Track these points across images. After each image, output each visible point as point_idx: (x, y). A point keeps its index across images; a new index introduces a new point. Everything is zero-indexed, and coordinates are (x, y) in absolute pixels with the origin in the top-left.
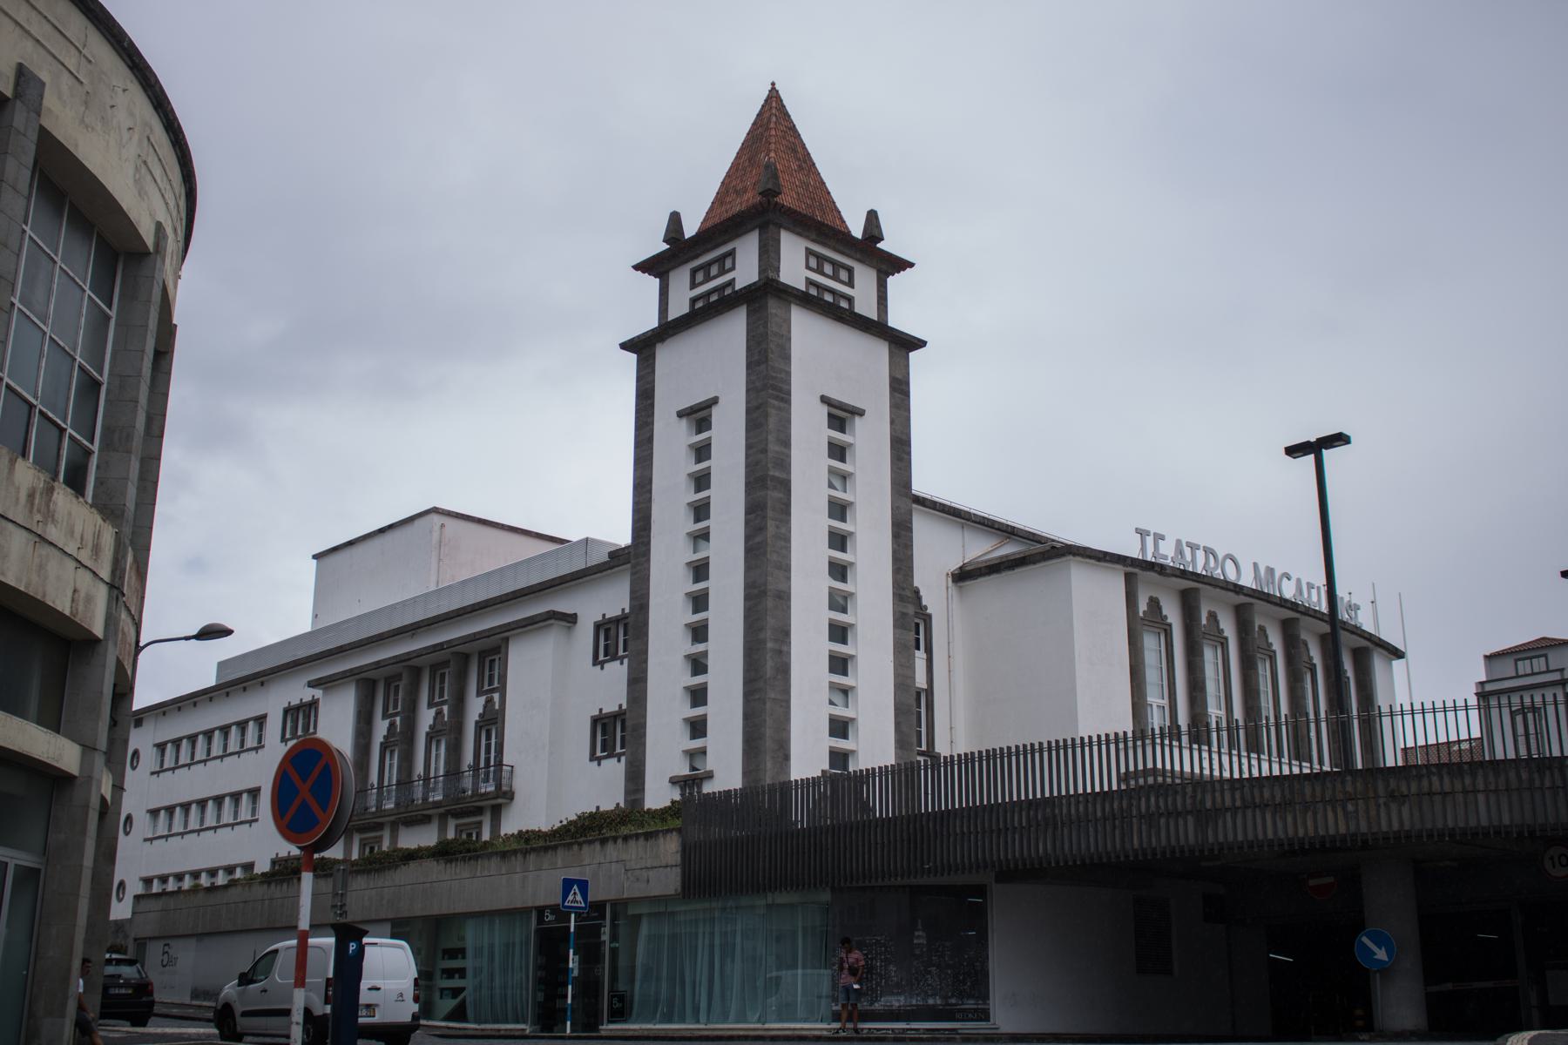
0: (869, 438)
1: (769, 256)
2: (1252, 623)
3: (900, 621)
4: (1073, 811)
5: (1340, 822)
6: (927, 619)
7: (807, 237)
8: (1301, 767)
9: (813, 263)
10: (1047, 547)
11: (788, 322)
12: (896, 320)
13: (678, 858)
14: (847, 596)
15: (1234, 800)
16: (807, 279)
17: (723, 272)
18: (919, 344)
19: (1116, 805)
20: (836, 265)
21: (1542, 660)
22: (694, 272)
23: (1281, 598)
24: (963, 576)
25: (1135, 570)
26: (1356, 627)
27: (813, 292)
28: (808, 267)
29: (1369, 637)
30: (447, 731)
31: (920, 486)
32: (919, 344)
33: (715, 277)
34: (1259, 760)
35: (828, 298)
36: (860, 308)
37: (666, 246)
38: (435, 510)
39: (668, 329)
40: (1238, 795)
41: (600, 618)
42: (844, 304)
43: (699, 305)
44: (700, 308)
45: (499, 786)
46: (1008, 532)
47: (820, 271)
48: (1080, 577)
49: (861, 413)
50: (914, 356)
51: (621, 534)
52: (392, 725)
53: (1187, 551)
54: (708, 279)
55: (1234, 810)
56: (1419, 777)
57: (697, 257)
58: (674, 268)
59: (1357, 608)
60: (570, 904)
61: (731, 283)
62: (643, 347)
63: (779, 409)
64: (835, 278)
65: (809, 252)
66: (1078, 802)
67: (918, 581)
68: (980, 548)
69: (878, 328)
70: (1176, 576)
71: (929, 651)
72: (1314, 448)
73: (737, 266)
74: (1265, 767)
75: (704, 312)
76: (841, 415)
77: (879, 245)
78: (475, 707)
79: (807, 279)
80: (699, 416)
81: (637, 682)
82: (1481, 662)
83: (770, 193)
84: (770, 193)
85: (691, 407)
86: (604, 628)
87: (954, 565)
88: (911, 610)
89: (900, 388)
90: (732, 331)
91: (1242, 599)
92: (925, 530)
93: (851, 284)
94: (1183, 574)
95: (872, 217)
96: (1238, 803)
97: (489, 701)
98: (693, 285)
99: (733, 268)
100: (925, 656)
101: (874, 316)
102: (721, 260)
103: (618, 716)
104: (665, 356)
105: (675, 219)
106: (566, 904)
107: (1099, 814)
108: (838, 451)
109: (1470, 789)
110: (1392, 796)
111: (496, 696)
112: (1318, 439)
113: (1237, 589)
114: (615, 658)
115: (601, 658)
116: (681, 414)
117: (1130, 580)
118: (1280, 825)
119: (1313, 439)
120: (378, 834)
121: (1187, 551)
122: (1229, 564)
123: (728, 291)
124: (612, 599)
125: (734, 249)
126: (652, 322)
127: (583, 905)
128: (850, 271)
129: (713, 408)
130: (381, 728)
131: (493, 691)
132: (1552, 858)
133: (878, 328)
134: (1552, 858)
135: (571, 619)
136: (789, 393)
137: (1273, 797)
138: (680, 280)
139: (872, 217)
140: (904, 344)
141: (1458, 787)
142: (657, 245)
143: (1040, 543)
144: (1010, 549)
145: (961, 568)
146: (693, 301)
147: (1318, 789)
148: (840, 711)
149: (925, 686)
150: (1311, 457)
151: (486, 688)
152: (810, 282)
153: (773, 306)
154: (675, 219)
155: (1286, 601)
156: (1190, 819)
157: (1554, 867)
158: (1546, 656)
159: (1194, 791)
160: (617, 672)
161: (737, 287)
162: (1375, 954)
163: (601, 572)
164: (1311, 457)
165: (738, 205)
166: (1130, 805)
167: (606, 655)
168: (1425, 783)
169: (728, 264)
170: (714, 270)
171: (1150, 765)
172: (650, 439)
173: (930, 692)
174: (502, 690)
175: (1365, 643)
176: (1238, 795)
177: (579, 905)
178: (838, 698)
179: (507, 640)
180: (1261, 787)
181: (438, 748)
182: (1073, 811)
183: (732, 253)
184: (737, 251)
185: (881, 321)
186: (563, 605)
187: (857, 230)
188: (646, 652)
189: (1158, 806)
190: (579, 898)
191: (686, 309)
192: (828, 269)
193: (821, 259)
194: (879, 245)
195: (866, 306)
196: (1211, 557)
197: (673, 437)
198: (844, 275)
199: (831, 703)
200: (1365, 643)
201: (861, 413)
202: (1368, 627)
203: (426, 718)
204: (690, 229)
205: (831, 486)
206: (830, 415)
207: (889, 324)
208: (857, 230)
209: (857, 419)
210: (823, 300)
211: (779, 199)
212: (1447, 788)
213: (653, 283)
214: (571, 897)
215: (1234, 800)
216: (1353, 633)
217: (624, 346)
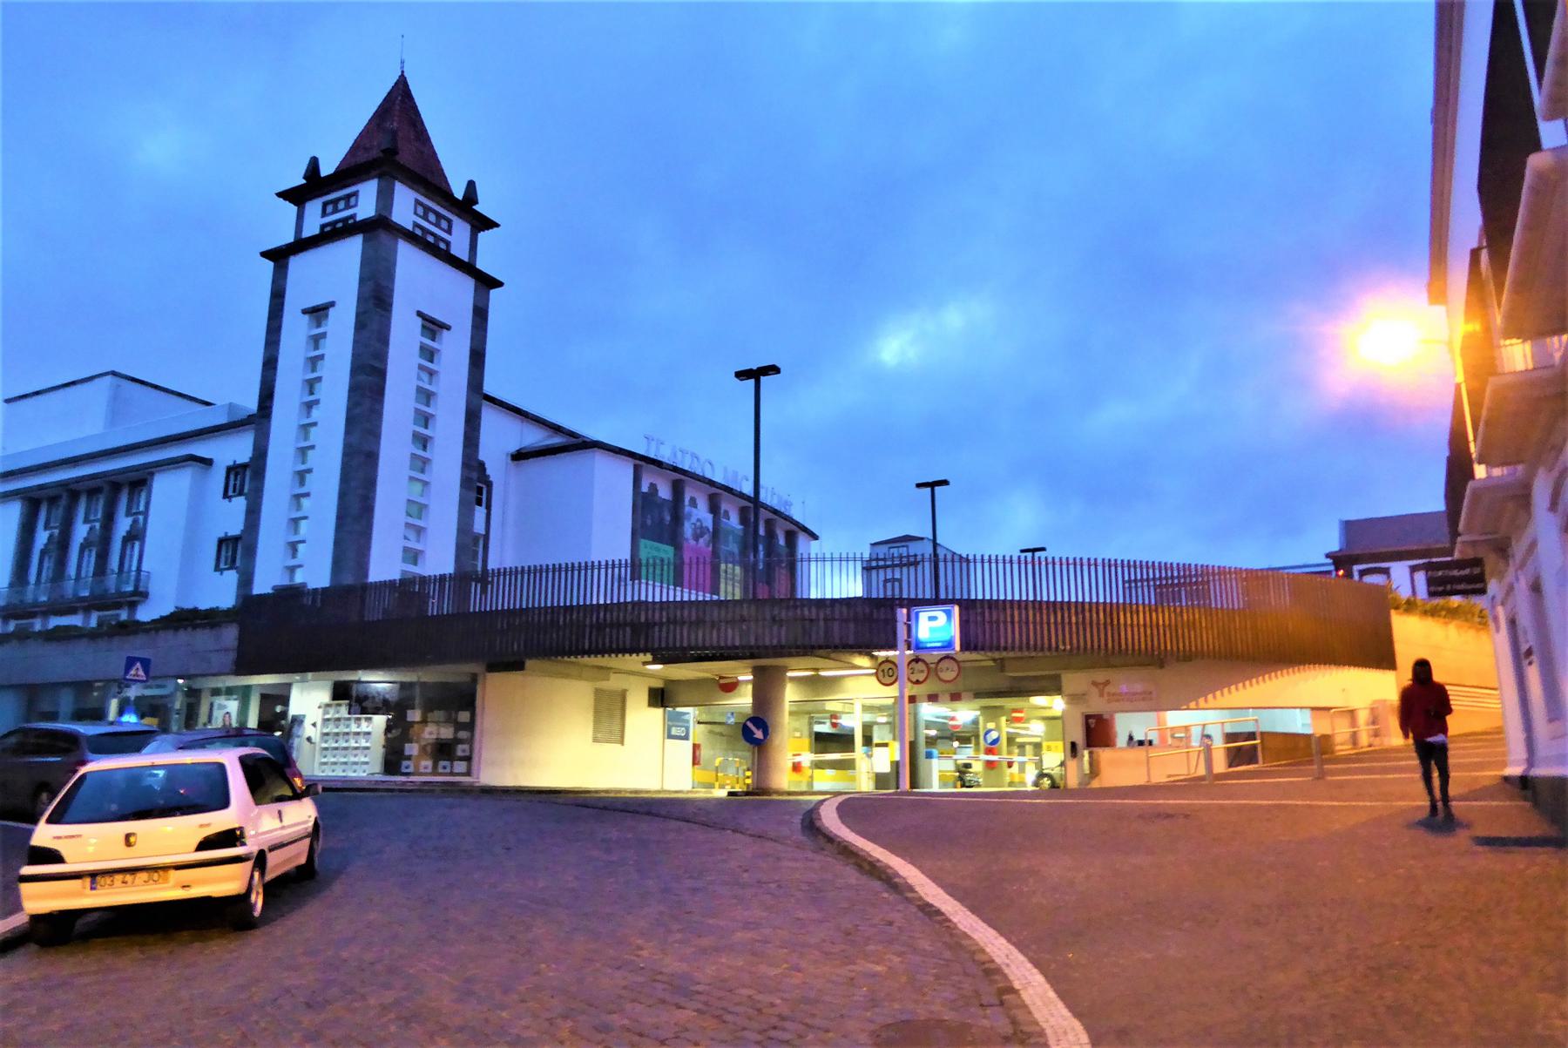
0: (454, 349)
1: (385, 198)
2: (719, 508)
3: (466, 483)
4: (542, 619)
5: (1195, 764)
6: (489, 485)
7: (417, 191)
8: (704, 596)
9: (420, 210)
10: (580, 440)
11: (395, 251)
12: (481, 265)
13: (236, 643)
14: (426, 461)
15: (661, 617)
16: (414, 222)
17: (348, 207)
18: (500, 284)
19: (574, 617)
20: (439, 216)
21: (905, 549)
22: (325, 205)
23: (741, 492)
24: (519, 456)
25: (642, 462)
26: (788, 516)
27: (419, 232)
28: (415, 213)
29: (796, 524)
30: (101, 543)
31: (489, 388)
32: (500, 284)
33: (341, 210)
34: (682, 591)
35: (431, 239)
36: (454, 251)
37: (304, 181)
38: (114, 373)
39: (301, 245)
40: (664, 614)
41: (231, 463)
42: (443, 246)
43: (328, 229)
44: (328, 232)
45: (136, 586)
46: (557, 429)
47: (425, 218)
48: (600, 460)
49: (448, 328)
50: (494, 293)
51: (251, 404)
52: (51, 536)
53: (679, 454)
54: (336, 211)
55: (661, 624)
56: (795, 607)
57: (328, 193)
58: (310, 199)
59: (791, 505)
60: (131, 677)
61: (353, 216)
62: (279, 257)
63: (382, 316)
64: (437, 225)
65: (417, 202)
66: (540, 613)
67: (483, 455)
68: (534, 437)
69: (468, 268)
70: (670, 470)
71: (489, 507)
72: (753, 374)
73: (359, 203)
74: (686, 595)
75: (330, 235)
76: (433, 326)
77: (474, 207)
78: (123, 525)
79: (414, 222)
80: (318, 312)
81: (253, 515)
82: (869, 546)
83: (391, 152)
84: (391, 152)
85: (314, 307)
86: (235, 470)
87: (513, 448)
88: (475, 475)
89: (480, 315)
90: (352, 249)
91: (714, 490)
92: (489, 416)
93: (449, 231)
94: (675, 469)
95: (471, 185)
96: (664, 620)
97: (135, 522)
98: (324, 214)
99: (356, 205)
100: (485, 511)
101: (465, 258)
102: (348, 197)
103: (236, 539)
104: (296, 263)
105: (314, 164)
106: (128, 677)
107: (561, 623)
108: (429, 354)
109: (830, 617)
110: (774, 619)
111: (141, 518)
112: (758, 368)
113: (712, 483)
114: (241, 493)
115: (230, 493)
116: (305, 312)
117: (637, 470)
118: (693, 637)
119: (755, 368)
120: (31, 621)
121: (679, 454)
122: (708, 467)
123: (351, 221)
124: (238, 449)
125: (358, 191)
126: (288, 237)
127: (145, 679)
128: (450, 222)
129: (331, 309)
130: (42, 537)
131: (139, 513)
132: (883, 671)
133: (468, 268)
134: (883, 671)
135: (208, 462)
136: (391, 305)
137: (690, 617)
138: (314, 208)
139: (471, 185)
140: (486, 283)
141: (822, 616)
142: (298, 180)
143: (574, 437)
144: (557, 440)
145: (518, 451)
146: (323, 226)
147: (723, 612)
148: (412, 545)
149: (484, 533)
150: (752, 382)
151: (134, 511)
152: (416, 225)
153: (383, 236)
154: (314, 164)
155: (744, 494)
156: (628, 630)
157: (884, 676)
158: (907, 547)
159: (633, 608)
160: (240, 503)
161: (358, 219)
162: (754, 734)
163: (242, 426)
164: (752, 382)
165: (362, 158)
166: (585, 617)
167: (234, 491)
168: (799, 611)
169: (353, 200)
170: (341, 205)
171: (643, 598)
172: (279, 328)
173: (486, 537)
174: (146, 513)
175: (794, 528)
176: (664, 614)
177: (141, 679)
178: (412, 535)
179: (152, 474)
180: (683, 608)
181: (90, 556)
182: (542, 619)
183: (355, 194)
184: (360, 193)
185: (471, 262)
186: (200, 449)
187: (459, 193)
188: (262, 491)
189: (605, 620)
190: (141, 672)
191: (317, 231)
192: (432, 217)
193: (427, 209)
194: (474, 207)
195: (460, 249)
196: (695, 459)
197: (295, 328)
198: (444, 224)
199: (406, 538)
200: (794, 528)
201: (448, 328)
202: (797, 517)
203: (81, 531)
204: (327, 169)
205: (419, 378)
206: (423, 326)
207: (477, 267)
208: (459, 193)
209: (445, 331)
210: (439, 248)
211: (397, 158)
212: (814, 617)
213: (291, 209)
214: (133, 672)
215: (661, 617)
216: (785, 519)
217: (265, 254)
